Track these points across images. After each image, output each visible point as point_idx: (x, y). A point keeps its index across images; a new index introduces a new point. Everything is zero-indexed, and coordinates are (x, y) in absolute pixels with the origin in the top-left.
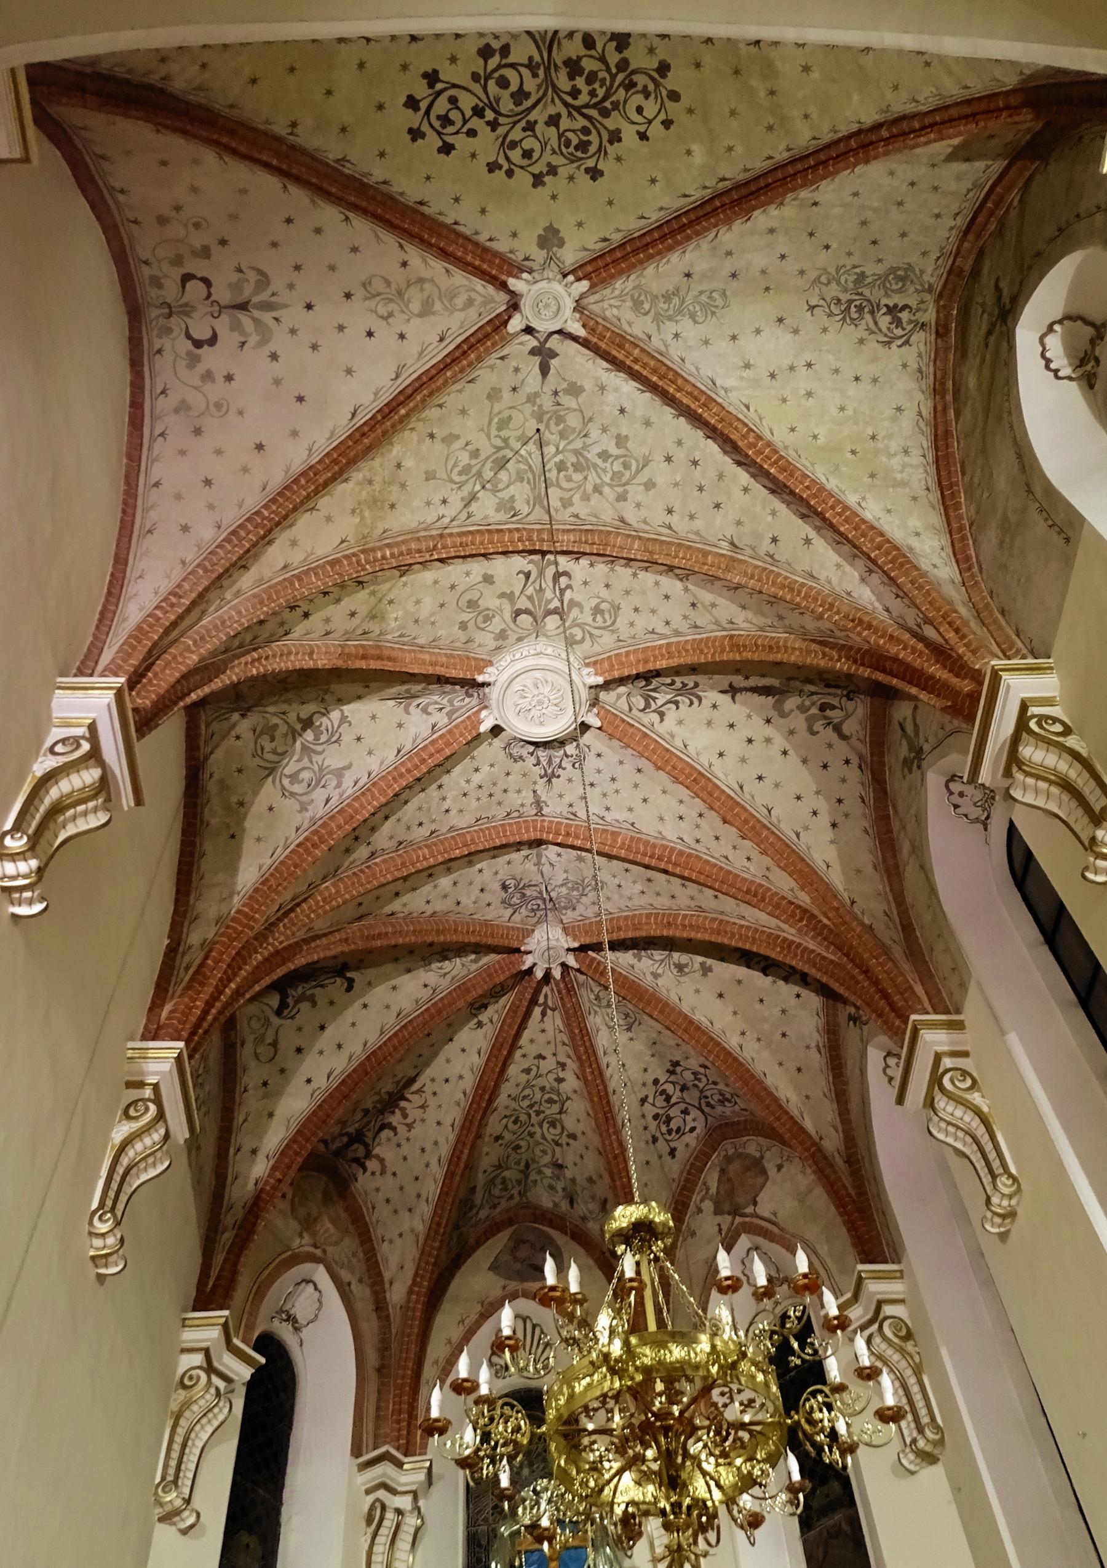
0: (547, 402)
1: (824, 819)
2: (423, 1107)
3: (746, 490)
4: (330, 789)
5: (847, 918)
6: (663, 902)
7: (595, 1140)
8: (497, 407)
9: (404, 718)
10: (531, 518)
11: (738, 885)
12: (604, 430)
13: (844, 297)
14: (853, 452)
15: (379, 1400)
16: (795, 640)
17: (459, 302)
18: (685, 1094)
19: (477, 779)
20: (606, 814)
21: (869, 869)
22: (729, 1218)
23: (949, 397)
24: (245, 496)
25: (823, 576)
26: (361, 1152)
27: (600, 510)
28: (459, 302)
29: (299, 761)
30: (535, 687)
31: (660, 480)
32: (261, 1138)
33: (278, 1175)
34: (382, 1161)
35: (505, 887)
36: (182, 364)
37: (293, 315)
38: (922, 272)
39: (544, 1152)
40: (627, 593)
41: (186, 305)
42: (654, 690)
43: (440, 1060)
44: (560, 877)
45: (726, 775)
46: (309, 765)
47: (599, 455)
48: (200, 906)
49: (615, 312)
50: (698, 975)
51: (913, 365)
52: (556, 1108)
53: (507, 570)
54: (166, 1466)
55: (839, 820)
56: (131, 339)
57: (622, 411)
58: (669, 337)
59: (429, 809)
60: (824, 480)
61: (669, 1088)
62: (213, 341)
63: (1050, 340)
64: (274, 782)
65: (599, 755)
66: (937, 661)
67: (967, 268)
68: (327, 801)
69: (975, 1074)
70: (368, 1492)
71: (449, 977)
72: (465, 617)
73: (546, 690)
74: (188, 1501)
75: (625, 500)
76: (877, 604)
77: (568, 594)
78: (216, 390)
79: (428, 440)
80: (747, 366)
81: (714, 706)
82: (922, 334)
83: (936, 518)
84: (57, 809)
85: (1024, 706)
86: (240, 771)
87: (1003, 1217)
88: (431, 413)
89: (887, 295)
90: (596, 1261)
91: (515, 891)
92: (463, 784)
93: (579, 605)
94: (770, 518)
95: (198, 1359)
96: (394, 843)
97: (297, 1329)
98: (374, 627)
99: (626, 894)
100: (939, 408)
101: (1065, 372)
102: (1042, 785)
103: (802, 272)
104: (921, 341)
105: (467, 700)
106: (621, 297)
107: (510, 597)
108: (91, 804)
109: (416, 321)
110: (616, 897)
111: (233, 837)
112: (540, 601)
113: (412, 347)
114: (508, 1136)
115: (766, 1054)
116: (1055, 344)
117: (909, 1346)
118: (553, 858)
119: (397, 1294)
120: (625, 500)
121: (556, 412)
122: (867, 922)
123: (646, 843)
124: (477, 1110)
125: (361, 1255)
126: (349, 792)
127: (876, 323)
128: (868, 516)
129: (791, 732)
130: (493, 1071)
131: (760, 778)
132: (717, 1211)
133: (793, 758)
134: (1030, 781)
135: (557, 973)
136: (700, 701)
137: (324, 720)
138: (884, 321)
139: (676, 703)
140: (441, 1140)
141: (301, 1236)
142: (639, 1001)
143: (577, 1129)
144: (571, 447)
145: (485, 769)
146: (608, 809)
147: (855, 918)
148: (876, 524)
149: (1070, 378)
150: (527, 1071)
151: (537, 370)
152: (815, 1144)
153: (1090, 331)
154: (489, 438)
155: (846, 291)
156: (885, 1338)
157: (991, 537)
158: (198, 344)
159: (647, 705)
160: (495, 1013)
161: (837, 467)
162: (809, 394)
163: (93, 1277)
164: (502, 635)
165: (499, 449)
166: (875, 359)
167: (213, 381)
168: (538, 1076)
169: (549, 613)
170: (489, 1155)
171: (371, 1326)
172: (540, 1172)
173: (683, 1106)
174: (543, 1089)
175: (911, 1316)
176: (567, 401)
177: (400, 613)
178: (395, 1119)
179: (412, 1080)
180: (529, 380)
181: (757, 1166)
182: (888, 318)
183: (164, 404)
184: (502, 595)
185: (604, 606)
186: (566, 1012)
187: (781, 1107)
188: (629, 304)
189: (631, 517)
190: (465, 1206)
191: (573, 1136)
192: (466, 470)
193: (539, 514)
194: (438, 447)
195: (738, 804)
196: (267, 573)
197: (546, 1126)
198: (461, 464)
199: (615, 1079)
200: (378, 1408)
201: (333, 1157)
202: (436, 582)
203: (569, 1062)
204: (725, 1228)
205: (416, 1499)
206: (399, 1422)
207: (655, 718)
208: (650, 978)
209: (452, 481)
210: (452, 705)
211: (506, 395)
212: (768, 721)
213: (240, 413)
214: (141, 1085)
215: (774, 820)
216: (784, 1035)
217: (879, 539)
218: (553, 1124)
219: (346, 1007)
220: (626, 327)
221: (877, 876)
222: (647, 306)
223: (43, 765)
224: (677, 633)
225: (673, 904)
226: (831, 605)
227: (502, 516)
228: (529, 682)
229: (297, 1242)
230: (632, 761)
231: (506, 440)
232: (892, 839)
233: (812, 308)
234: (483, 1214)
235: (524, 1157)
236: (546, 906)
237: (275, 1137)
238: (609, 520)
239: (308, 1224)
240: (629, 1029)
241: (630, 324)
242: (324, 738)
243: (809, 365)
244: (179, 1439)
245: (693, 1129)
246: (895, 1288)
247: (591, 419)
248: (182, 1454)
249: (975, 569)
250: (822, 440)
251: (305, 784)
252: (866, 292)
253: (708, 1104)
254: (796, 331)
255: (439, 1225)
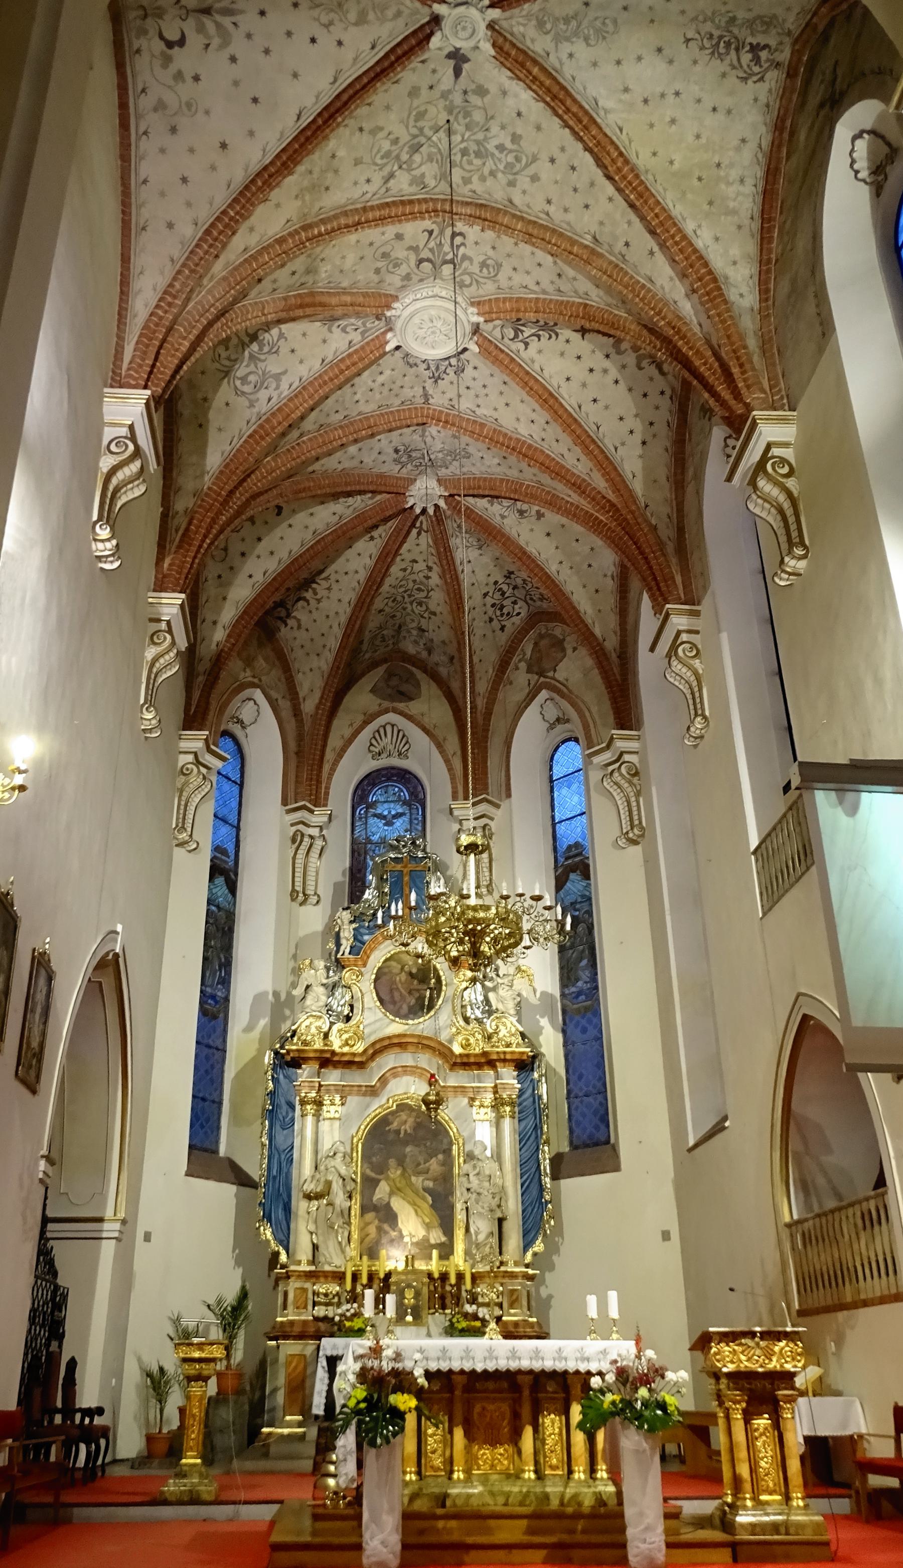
0: (457, 99)
1: (638, 438)
2: (329, 589)
3: (610, 199)
4: (271, 389)
5: (640, 520)
6: (513, 474)
7: (449, 619)
8: (416, 103)
9: (328, 335)
10: (437, 190)
11: (568, 477)
12: (503, 127)
13: (716, 33)
14: (700, 179)
15: (297, 772)
16: (632, 323)
17: (390, 13)
18: (516, 591)
19: (381, 379)
20: (477, 409)
21: (663, 480)
22: (536, 677)
23: (786, 135)
24: (215, 194)
25: (658, 284)
26: (283, 613)
27: (494, 191)
28: (390, 13)
29: (247, 366)
30: (429, 322)
31: (544, 176)
32: (219, 613)
33: (232, 641)
34: (298, 621)
35: (397, 451)
36: (157, 63)
37: (249, 20)
38: (784, 21)
39: (413, 621)
40: (509, 256)
41: (158, 8)
42: (523, 325)
43: (342, 560)
44: (439, 446)
45: (569, 396)
46: (254, 369)
47: (497, 147)
48: (181, 481)
49: (522, 29)
50: (534, 519)
51: (763, 99)
52: (424, 594)
53: (414, 230)
54: (177, 819)
55: (649, 439)
56: (115, 42)
57: (519, 114)
58: (564, 57)
59: (343, 401)
60: (671, 206)
61: (505, 587)
62: (182, 42)
63: (858, 143)
64: (229, 383)
65: (475, 368)
66: (725, 381)
67: (821, 28)
68: (270, 400)
69: (700, 647)
70: (292, 825)
71: (351, 508)
72: (379, 264)
73: (439, 324)
74: (191, 836)
75: (514, 186)
76: (694, 318)
77: (462, 250)
78: (186, 89)
79: (358, 133)
80: (626, 90)
81: (568, 341)
82: (776, 72)
83: (752, 247)
84: (117, 490)
85: (769, 447)
86: (203, 373)
87: (696, 738)
88: (363, 111)
89: (753, 35)
90: (444, 692)
91: (404, 454)
92: (370, 383)
93: (470, 259)
94: (626, 226)
95: (190, 758)
96: (317, 426)
97: (244, 728)
98: (310, 279)
99: (485, 463)
100: (776, 143)
101: (863, 174)
102: (767, 505)
103: (683, 12)
104: (774, 78)
105: (377, 322)
106: (528, 16)
107: (415, 249)
108: (136, 483)
109: (353, 30)
110: (478, 464)
111: (200, 426)
112: (439, 253)
113: (347, 54)
114: (387, 609)
115: (575, 578)
116: (862, 145)
117: (635, 780)
118: (434, 433)
119: (309, 707)
120: (514, 186)
121: (464, 108)
122: (654, 522)
123: (506, 435)
124: (367, 595)
125: (283, 680)
126: (286, 393)
127: (739, 59)
128: (699, 244)
129: (624, 367)
130: (380, 571)
131: (595, 401)
132: (529, 671)
133: (622, 386)
134: (760, 501)
135: (431, 511)
136: (557, 335)
137: (267, 335)
138: (746, 57)
139: (539, 337)
140: (341, 611)
141: (244, 670)
142: (487, 533)
143: (438, 610)
144: (473, 138)
145: (388, 372)
146: (478, 406)
147: (646, 521)
148: (704, 253)
149: (864, 181)
150: (405, 570)
151: (451, 71)
152: (599, 644)
153: (886, 150)
154: (407, 127)
155: (718, 28)
156: (621, 775)
157: (784, 287)
158: (170, 45)
159: (516, 336)
160: (383, 532)
161: (684, 193)
162: (673, 121)
163: (143, 739)
164: (407, 277)
165: (415, 137)
166: (731, 93)
167: (184, 81)
168: (412, 573)
169: (445, 262)
170: (373, 622)
171: (291, 725)
172: (409, 632)
173: (513, 599)
174: (414, 581)
175: (640, 762)
176: (474, 99)
177: (329, 267)
178: (309, 595)
179: (321, 572)
180: (444, 79)
181: (559, 644)
182: (750, 56)
183: (146, 102)
184: (410, 248)
185: (489, 262)
186: (435, 535)
187: (580, 617)
188: (534, 22)
189: (517, 200)
190: (356, 652)
191: (434, 614)
192: (387, 155)
193: (444, 187)
194: (365, 138)
195: (576, 420)
196: (232, 257)
197: (415, 604)
198: (383, 151)
199: (466, 580)
200: (297, 776)
201: (268, 619)
202: (358, 241)
203: (435, 567)
204: (532, 683)
205: (321, 830)
206: (310, 785)
207: (521, 346)
208: (499, 518)
209: (376, 164)
210: (364, 325)
211: (424, 92)
212: (607, 356)
213: (207, 112)
214: (159, 621)
215: (601, 435)
216: (590, 566)
217: (703, 271)
218: (420, 604)
219: (277, 525)
220: (529, 43)
221: (667, 485)
222: (548, 26)
223: (106, 463)
224: (544, 292)
225: (521, 476)
226: (660, 311)
227: (414, 189)
228: (426, 318)
229: (242, 675)
230: (500, 376)
231: (421, 130)
232: (684, 459)
233: (688, 41)
234: (367, 656)
235: (398, 622)
236: (428, 464)
237: (228, 614)
238: (499, 199)
239: (249, 662)
240: (480, 548)
241: (533, 41)
242: (266, 349)
243: (677, 94)
244: (183, 803)
245: (518, 614)
246: (634, 745)
247: (492, 118)
248: (185, 810)
249: (770, 302)
250: (676, 165)
251: (252, 385)
252: (736, 31)
253: (531, 599)
254: (671, 62)
255: (338, 668)
